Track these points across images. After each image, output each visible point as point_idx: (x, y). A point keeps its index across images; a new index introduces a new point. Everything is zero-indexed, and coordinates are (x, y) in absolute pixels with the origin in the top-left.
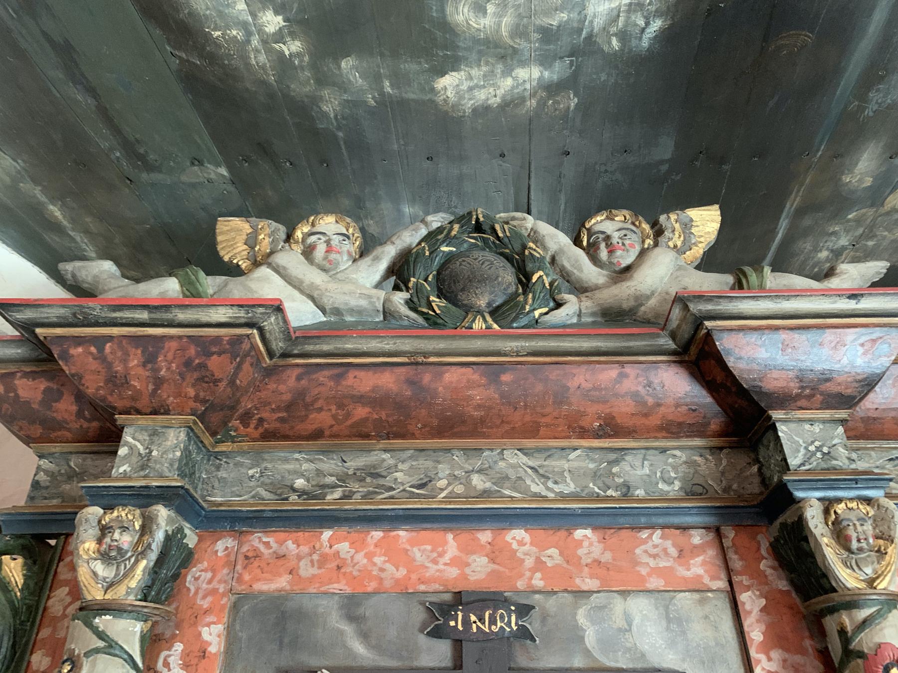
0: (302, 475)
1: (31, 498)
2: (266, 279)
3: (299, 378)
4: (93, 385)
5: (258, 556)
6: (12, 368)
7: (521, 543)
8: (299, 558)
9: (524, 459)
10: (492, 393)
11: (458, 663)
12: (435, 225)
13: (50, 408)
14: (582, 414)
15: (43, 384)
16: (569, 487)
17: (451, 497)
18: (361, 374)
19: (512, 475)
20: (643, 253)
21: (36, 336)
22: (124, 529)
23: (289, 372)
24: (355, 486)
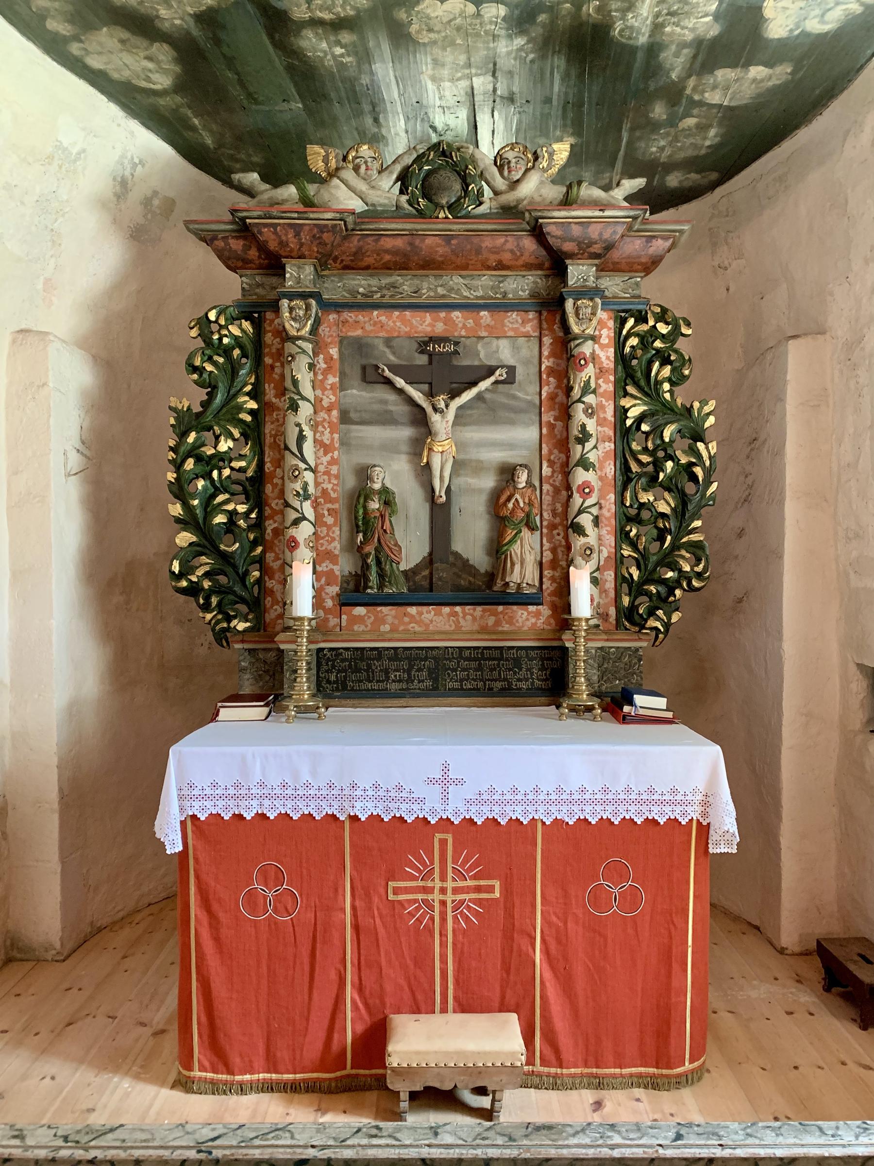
0: (362, 287)
1: (243, 295)
2: (337, 187)
3: (359, 241)
4: (273, 245)
5: (347, 321)
6: (227, 234)
7: (457, 317)
8: (365, 323)
9: (462, 280)
10: (447, 249)
11: (430, 362)
12: (421, 151)
13: (246, 254)
14: (487, 259)
15: (241, 242)
16: (480, 293)
17: (429, 297)
18: (388, 239)
19: (456, 288)
20: (527, 170)
21: (246, 223)
22: (299, 309)
23: (353, 238)
24: (385, 292)
